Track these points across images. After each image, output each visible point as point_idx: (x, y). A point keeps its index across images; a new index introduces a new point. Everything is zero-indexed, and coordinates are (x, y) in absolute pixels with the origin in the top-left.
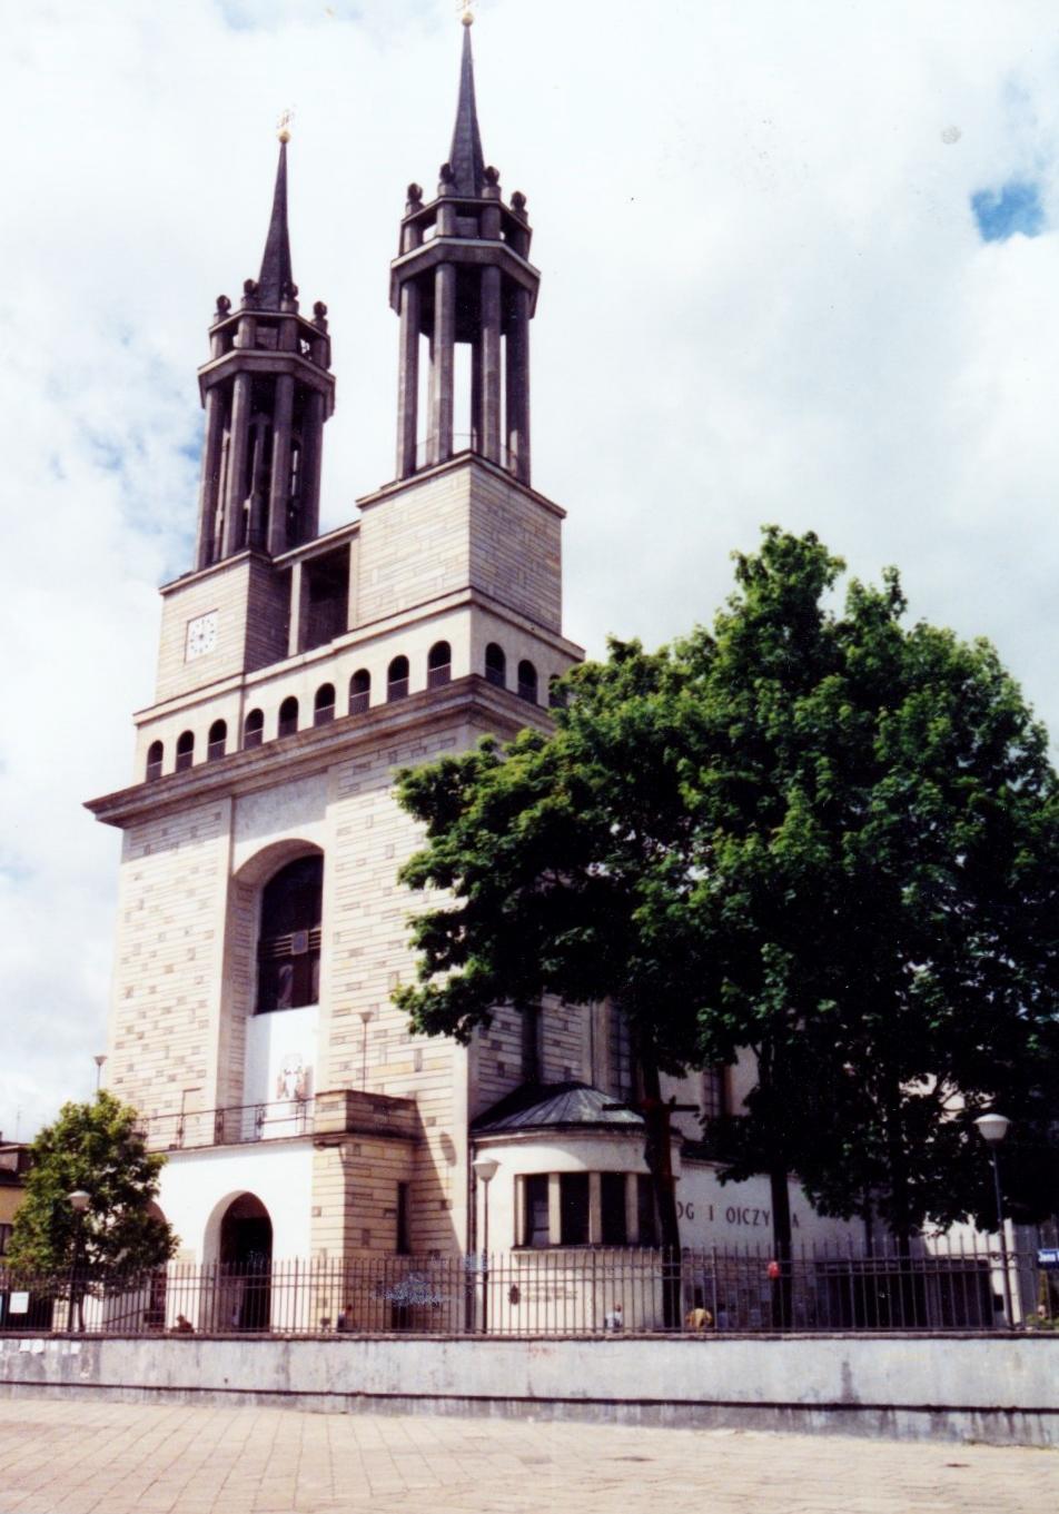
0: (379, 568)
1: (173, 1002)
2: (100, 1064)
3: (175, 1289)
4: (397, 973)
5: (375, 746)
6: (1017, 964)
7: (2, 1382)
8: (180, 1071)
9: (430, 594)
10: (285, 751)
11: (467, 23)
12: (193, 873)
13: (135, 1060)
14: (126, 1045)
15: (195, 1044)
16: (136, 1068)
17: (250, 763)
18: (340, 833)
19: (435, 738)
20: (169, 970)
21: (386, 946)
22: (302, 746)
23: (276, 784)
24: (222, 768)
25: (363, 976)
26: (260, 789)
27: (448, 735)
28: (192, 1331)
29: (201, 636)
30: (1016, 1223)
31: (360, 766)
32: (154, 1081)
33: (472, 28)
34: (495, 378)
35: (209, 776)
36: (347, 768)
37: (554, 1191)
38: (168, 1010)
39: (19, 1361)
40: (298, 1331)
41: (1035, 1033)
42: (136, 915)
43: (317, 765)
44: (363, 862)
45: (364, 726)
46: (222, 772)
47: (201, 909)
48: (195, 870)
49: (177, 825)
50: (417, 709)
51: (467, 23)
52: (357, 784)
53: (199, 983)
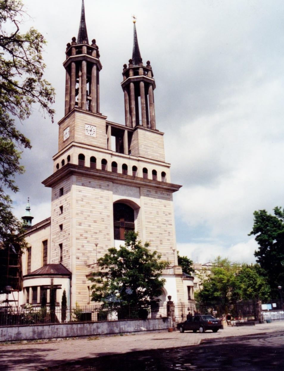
0: (144, 145)
1: (98, 231)
2: (96, 246)
3: (176, 308)
4: (161, 240)
5: (154, 188)
6: (16, 243)
7: (1, 342)
8: (102, 251)
9: (154, 158)
10: (136, 180)
11: (134, 23)
12: (101, 198)
13: (84, 244)
14: (80, 239)
15: (106, 245)
16: (85, 247)
17: (126, 178)
18: (145, 204)
19: (166, 193)
20: (95, 222)
21: (159, 234)
22: (141, 181)
23: (125, 185)
24: (119, 176)
25: (154, 239)
26: (121, 184)
27: (168, 193)
28: (59, 322)
29: (91, 131)
30: (46, 304)
31: (149, 191)
32: (92, 252)
33: (136, 24)
34: (142, 109)
35: (114, 176)
36: (145, 190)
37: (39, 289)
38: (96, 233)
39: (280, 315)
40: (112, 320)
41: (138, 267)
42: (80, 202)
43: (139, 186)
44: (151, 213)
45: (157, 184)
46: (118, 177)
47: (105, 208)
48: (102, 197)
49: (94, 182)
50: (169, 186)
51: (134, 23)
52: (148, 195)
53: (106, 228)
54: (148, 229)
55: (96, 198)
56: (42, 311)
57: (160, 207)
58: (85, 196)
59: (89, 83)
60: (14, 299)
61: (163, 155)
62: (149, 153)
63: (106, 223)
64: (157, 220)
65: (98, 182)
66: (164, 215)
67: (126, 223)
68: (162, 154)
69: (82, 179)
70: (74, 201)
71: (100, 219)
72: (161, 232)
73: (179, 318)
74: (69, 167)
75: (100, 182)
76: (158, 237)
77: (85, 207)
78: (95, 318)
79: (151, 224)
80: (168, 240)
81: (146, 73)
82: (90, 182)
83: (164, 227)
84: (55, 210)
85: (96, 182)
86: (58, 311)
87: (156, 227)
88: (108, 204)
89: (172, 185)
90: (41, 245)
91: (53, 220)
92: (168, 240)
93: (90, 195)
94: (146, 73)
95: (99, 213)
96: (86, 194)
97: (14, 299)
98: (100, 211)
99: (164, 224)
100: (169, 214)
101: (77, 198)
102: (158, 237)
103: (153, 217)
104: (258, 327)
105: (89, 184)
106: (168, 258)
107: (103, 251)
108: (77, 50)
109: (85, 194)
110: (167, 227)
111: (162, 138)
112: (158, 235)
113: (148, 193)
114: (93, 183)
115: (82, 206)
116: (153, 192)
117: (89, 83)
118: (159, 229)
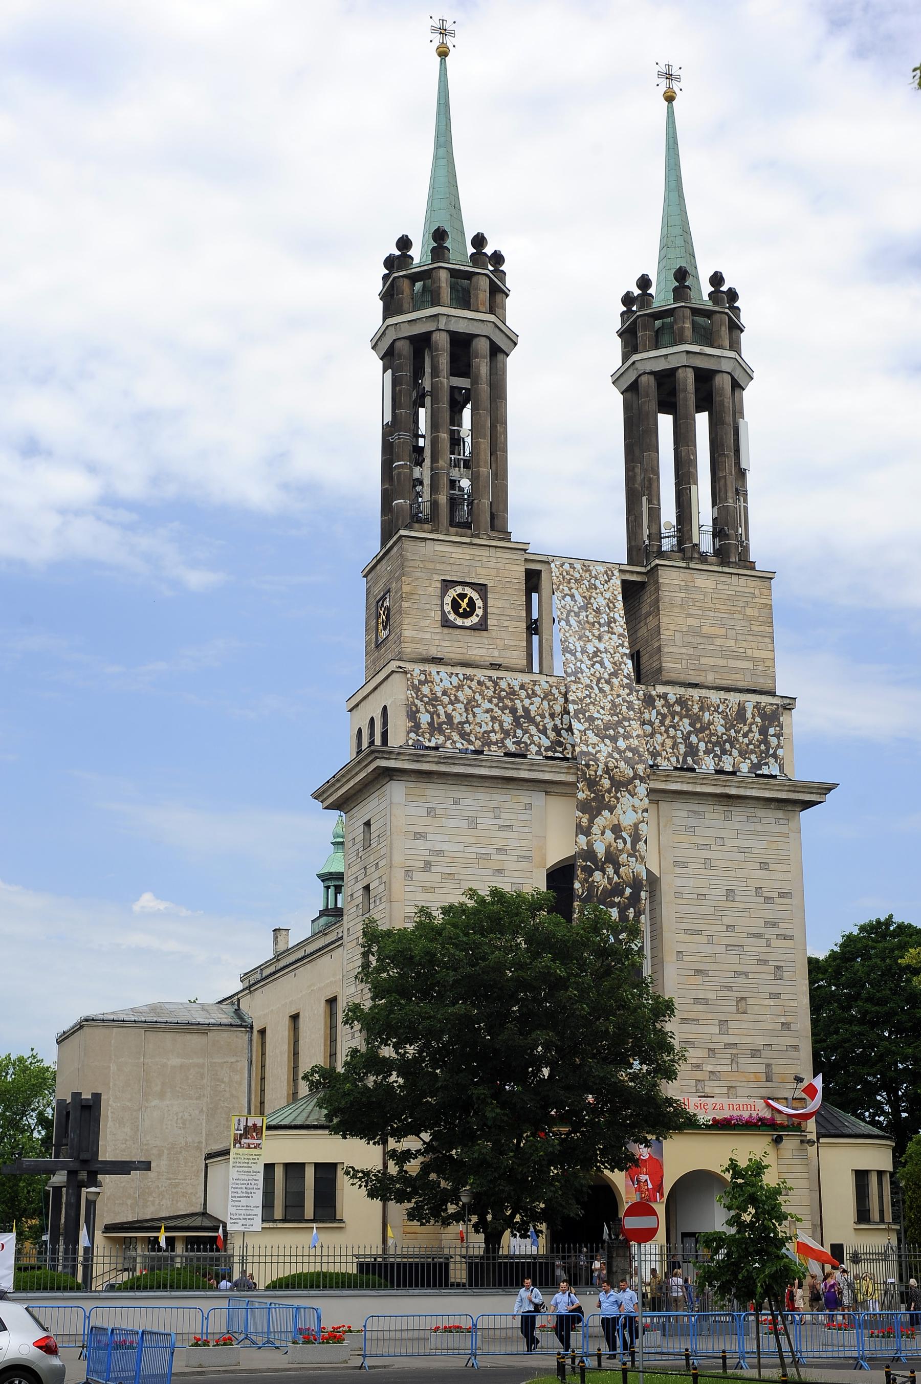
4: (743, 999)
18: (677, 864)
21: (732, 974)
25: (711, 995)
55: (480, 857)
56: (625, 906)
57: (740, 873)
58: (440, 853)
59: (390, 370)
61: (768, 663)
62: (703, 661)
64: (727, 921)
65: (487, 796)
66: (762, 900)
68: (764, 660)
69: (428, 792)
70: (399, 874)
74: (376, 758)
75: (496, 797)
76: (730, 988)
78: (458, 1272)
80: (775, 996)
82: (456, 802)
83: (754, 947)
84: (352, 895)
85: (481, 796)
87: (722, 949)
89: (808, 787)
90: (286, 1022)
91: (348, 929)
92: (775, 996)
93: (456, 847)
96: (445, 847)
99: (759, 936)
100: (782, 895)
102: (730, 988)
103: (711, 910)
104: (753, 715)
105: (454, 807)
109: (438, 847)
111: (765, 592)
113: (691, 822)
114: (469, 802)
115: (425, 889)
116: (712, 816)
117: (390, 370)
118: (735, 959)
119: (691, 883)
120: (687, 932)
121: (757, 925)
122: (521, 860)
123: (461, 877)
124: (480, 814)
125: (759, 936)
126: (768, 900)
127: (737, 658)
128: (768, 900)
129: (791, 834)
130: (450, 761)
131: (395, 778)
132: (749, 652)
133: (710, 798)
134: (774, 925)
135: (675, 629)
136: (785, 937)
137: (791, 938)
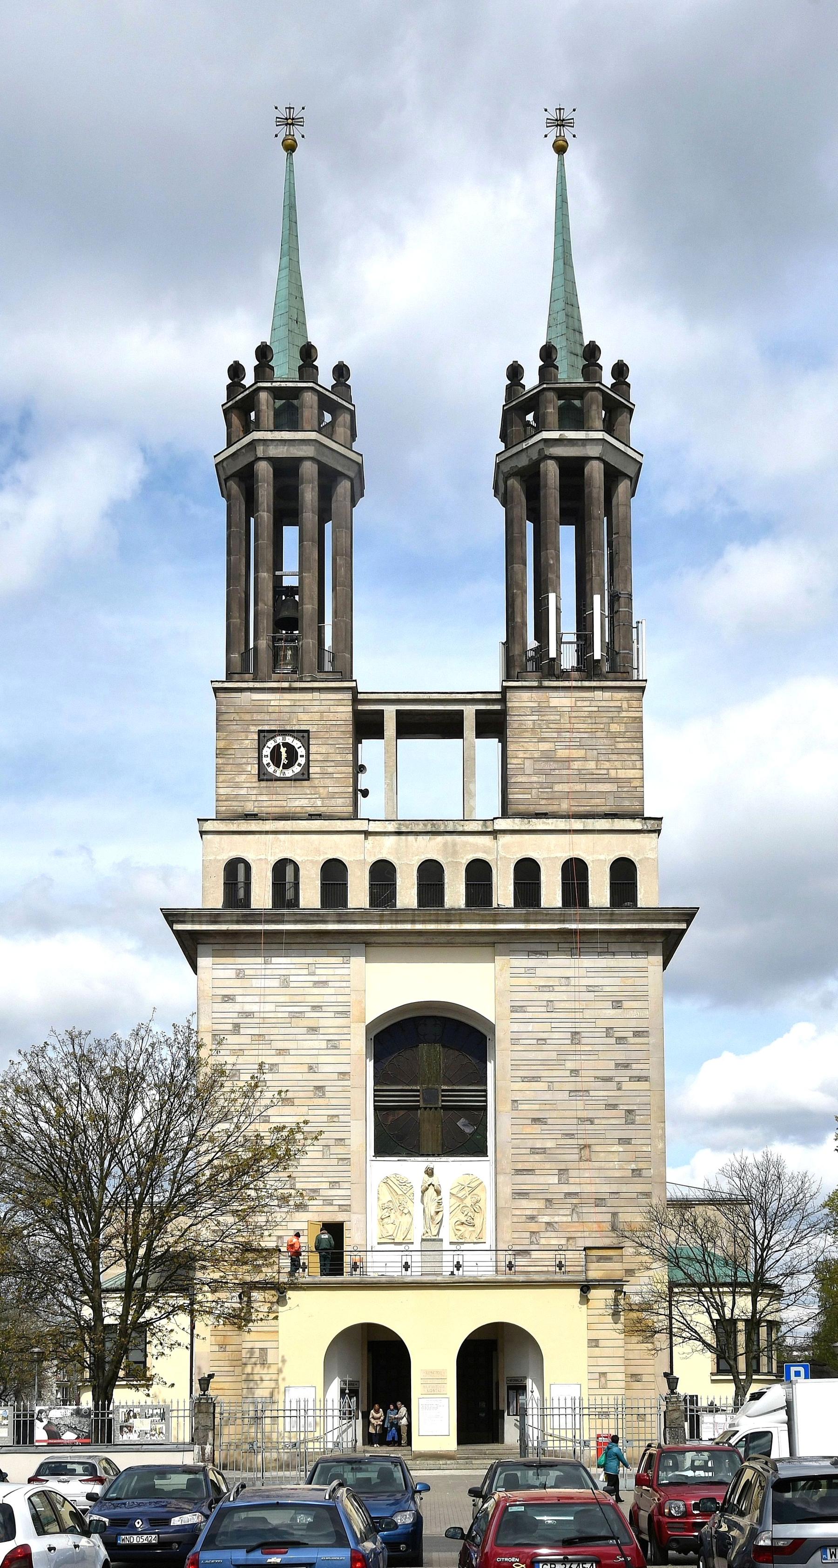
18: (514, 1009)
54: (521, 1107)
55: (294, 1015)
58: (248, 1015)
60: (781, 1408)
61: (636, 783)
63: (334, 1102)
64: (570, 1065)
66: (613, 1041)
67: (443, 1091)
71: (312, 1088)
72: (585, 1114)
73: (563, 1418)
76: (571, 1136)
77: (246, 1052)
79: (543, 1086)
81: (328, 418)
86: (605, 1426)
88: (346, 1030)
93: (270, 1007)
94: (328, 418)
95: (305, 1068)
96: (254, 1008)
97: (781, 1408)
98: (308, 1060)
100: (637, 1034)
101: (216, 1027)
102: (571, 1136)
103: (554, 1055)
106: (615, 1215)
107: (321, 1202)
108: (279, 403)
109: (248, 1008)
110: (619, 1089)
112: (571, 1129)
119: (530, 1027)
120: (524, 1079)
121: (606, 1067)
122: (338, 1016)
123: (272, 1037)
124: (293, 972)
125: (609, 1079)
126: (621, 1040)
127: (598, 781)
128: (621, 1040)
129: (650, 969)
130: (250, 919)
131: (200, 941)
132: (613, 773)
133: (553, 937)
134: (626, 1066)
135: (525, 756)
136: (639, 1079)
137: (646, 1079)
